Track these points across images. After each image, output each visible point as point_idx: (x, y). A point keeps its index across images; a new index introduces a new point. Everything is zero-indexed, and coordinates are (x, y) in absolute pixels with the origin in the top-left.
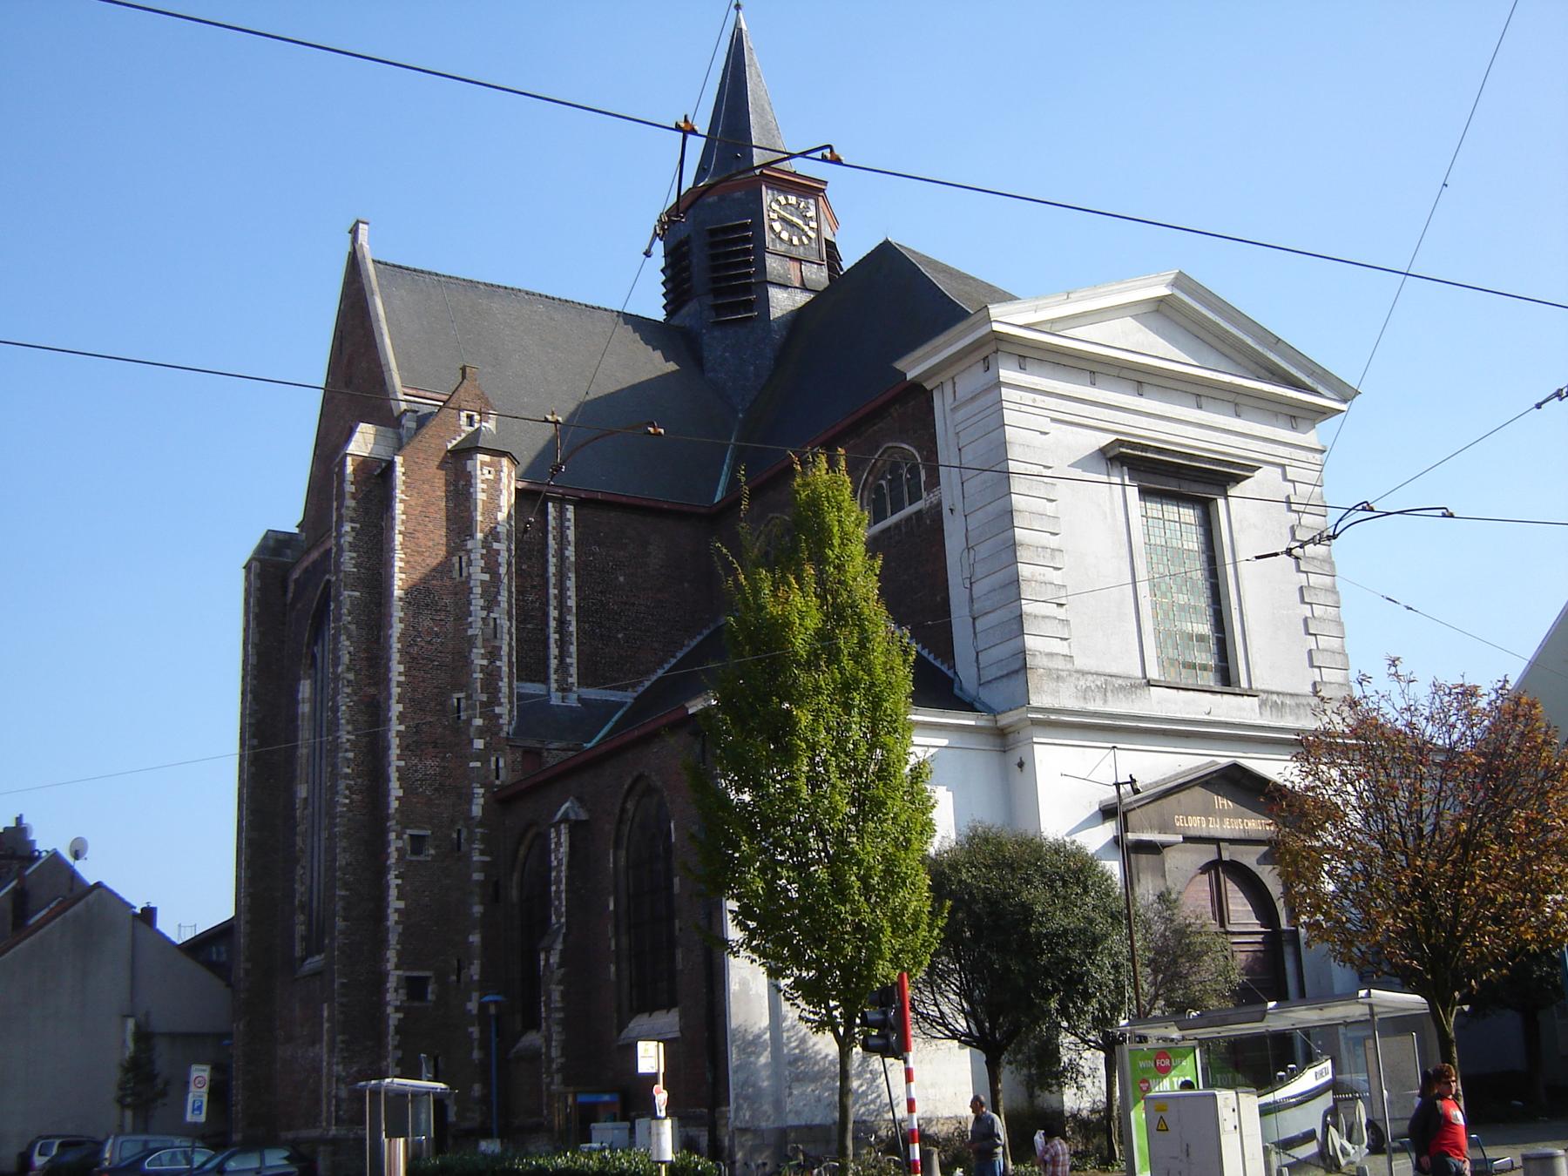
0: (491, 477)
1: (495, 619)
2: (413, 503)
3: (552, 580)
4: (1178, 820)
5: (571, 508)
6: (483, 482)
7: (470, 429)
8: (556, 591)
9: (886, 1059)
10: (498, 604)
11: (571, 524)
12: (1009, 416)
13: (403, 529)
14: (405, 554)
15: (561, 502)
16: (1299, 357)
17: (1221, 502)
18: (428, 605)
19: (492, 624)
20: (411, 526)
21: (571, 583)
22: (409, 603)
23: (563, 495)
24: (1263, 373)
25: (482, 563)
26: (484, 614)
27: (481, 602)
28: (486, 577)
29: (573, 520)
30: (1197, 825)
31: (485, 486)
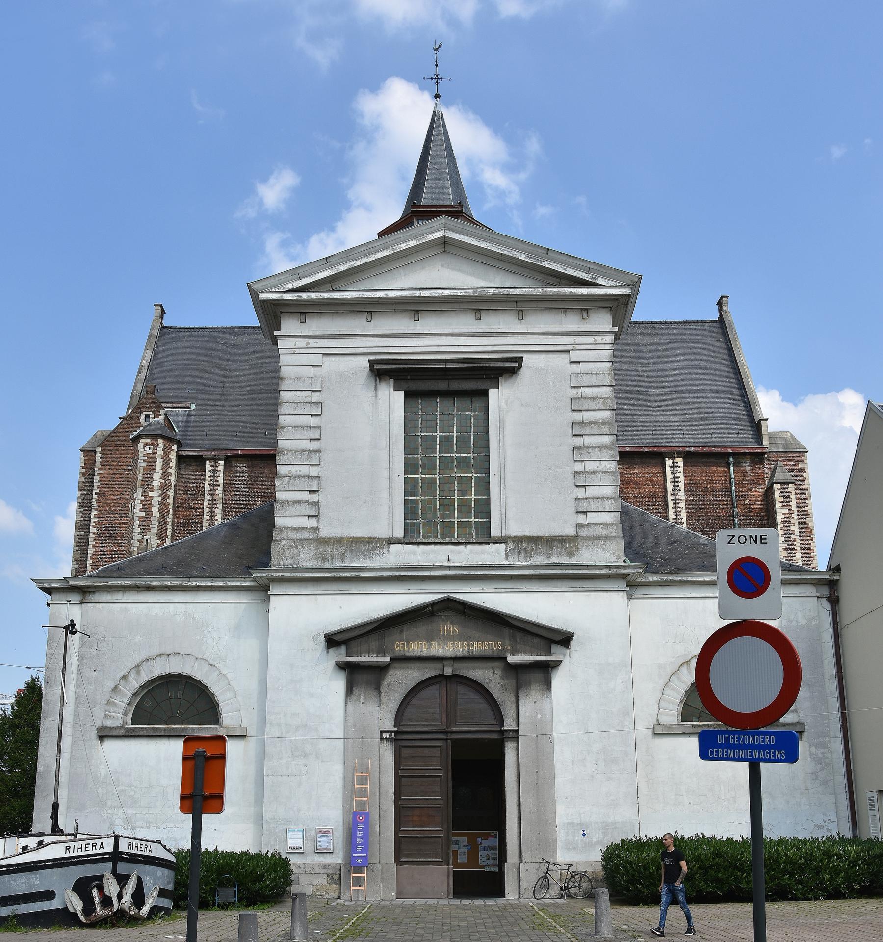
0: (151, 452)
1: (147, 540)
2: (105, 475)
3: (206, 510)
4: (398, 645)
5: (222, 463)
6: (145, 455)
7: (146, 424)
8: (208, 517)
9: (113, 838)
10: (150, 530)
11: (221, 474)
12: (283, 359)
13: (98, 491)
14: (99, 507)
15: (215, 459)
16: (571, 260)
17: (492, 393)
18: (111, 535)
19: (145, 543)
20: (105, 488)
21: (219, 512)
22: (99, 535)
23: (215, 455)
24: (551, 280)
25: (141, 506)
26: (140, 537)
27: (139, 530)
28: (143, 514)
29: (222, 471)
30: (418, 648)
31: (146, 458)
